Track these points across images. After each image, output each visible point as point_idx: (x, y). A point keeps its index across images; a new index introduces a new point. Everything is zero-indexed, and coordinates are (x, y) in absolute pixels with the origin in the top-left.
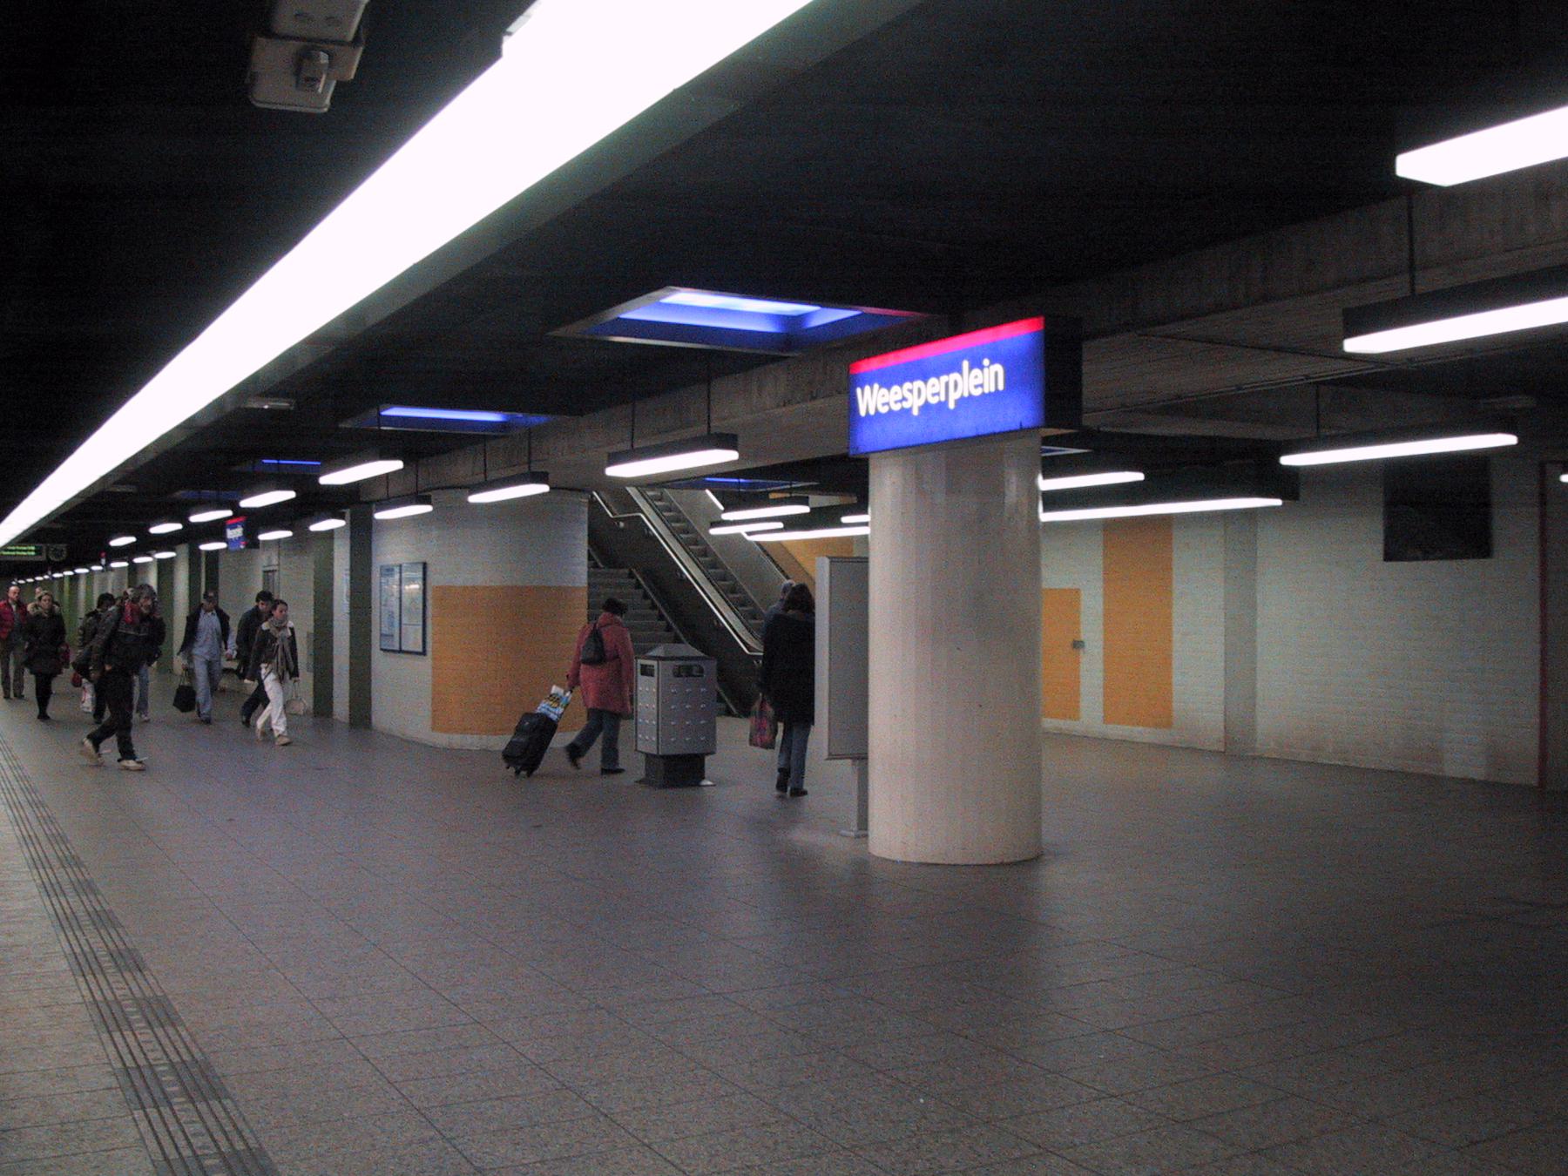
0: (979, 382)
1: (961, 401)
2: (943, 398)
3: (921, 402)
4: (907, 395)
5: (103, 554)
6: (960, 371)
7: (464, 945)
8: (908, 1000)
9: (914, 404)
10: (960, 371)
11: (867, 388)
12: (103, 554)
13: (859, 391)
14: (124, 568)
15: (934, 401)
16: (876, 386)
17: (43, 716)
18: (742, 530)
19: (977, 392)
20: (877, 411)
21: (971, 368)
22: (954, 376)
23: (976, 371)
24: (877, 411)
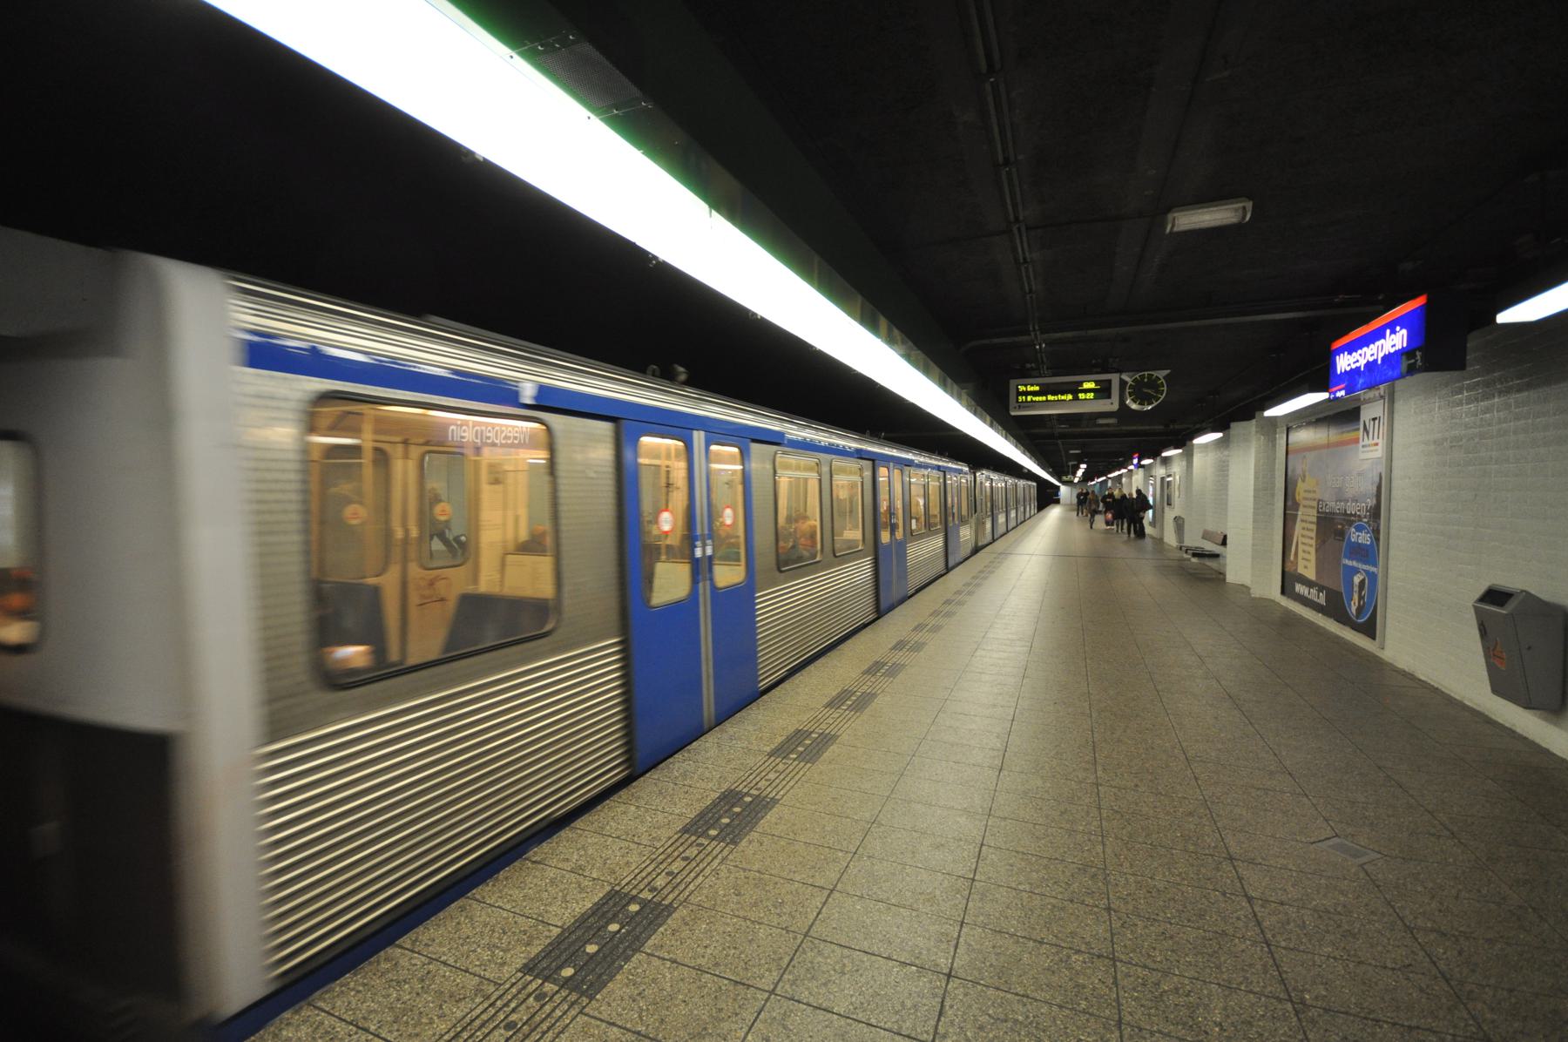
0: (1393, 343)
1: (1385, 358)
2: (1375, 358)
3: (1365, 362)
4: (1359, 358)
5: (1137, 455)
6: (1384, 338)
7: (1278, 850)
8: (375, 974)
9: (1362, 362)
10: (1384, 338)
11: (1342, 355)
12: (1137, 455)
13: (1337, 357)
14: (715, 463)
15: (1371, 359)
16: (1346, 353)
17: (1091, 527)
18: (787, 460)
19: (1392, 350)
20: (1345, 371)
21: (1391, 334)
22: (1382, 341)
23: (1393, 336)
24: (1345, 371)
